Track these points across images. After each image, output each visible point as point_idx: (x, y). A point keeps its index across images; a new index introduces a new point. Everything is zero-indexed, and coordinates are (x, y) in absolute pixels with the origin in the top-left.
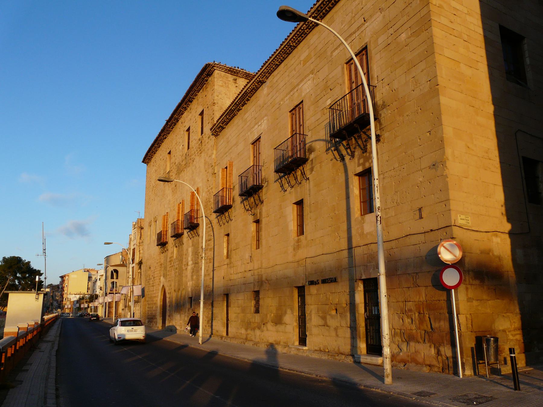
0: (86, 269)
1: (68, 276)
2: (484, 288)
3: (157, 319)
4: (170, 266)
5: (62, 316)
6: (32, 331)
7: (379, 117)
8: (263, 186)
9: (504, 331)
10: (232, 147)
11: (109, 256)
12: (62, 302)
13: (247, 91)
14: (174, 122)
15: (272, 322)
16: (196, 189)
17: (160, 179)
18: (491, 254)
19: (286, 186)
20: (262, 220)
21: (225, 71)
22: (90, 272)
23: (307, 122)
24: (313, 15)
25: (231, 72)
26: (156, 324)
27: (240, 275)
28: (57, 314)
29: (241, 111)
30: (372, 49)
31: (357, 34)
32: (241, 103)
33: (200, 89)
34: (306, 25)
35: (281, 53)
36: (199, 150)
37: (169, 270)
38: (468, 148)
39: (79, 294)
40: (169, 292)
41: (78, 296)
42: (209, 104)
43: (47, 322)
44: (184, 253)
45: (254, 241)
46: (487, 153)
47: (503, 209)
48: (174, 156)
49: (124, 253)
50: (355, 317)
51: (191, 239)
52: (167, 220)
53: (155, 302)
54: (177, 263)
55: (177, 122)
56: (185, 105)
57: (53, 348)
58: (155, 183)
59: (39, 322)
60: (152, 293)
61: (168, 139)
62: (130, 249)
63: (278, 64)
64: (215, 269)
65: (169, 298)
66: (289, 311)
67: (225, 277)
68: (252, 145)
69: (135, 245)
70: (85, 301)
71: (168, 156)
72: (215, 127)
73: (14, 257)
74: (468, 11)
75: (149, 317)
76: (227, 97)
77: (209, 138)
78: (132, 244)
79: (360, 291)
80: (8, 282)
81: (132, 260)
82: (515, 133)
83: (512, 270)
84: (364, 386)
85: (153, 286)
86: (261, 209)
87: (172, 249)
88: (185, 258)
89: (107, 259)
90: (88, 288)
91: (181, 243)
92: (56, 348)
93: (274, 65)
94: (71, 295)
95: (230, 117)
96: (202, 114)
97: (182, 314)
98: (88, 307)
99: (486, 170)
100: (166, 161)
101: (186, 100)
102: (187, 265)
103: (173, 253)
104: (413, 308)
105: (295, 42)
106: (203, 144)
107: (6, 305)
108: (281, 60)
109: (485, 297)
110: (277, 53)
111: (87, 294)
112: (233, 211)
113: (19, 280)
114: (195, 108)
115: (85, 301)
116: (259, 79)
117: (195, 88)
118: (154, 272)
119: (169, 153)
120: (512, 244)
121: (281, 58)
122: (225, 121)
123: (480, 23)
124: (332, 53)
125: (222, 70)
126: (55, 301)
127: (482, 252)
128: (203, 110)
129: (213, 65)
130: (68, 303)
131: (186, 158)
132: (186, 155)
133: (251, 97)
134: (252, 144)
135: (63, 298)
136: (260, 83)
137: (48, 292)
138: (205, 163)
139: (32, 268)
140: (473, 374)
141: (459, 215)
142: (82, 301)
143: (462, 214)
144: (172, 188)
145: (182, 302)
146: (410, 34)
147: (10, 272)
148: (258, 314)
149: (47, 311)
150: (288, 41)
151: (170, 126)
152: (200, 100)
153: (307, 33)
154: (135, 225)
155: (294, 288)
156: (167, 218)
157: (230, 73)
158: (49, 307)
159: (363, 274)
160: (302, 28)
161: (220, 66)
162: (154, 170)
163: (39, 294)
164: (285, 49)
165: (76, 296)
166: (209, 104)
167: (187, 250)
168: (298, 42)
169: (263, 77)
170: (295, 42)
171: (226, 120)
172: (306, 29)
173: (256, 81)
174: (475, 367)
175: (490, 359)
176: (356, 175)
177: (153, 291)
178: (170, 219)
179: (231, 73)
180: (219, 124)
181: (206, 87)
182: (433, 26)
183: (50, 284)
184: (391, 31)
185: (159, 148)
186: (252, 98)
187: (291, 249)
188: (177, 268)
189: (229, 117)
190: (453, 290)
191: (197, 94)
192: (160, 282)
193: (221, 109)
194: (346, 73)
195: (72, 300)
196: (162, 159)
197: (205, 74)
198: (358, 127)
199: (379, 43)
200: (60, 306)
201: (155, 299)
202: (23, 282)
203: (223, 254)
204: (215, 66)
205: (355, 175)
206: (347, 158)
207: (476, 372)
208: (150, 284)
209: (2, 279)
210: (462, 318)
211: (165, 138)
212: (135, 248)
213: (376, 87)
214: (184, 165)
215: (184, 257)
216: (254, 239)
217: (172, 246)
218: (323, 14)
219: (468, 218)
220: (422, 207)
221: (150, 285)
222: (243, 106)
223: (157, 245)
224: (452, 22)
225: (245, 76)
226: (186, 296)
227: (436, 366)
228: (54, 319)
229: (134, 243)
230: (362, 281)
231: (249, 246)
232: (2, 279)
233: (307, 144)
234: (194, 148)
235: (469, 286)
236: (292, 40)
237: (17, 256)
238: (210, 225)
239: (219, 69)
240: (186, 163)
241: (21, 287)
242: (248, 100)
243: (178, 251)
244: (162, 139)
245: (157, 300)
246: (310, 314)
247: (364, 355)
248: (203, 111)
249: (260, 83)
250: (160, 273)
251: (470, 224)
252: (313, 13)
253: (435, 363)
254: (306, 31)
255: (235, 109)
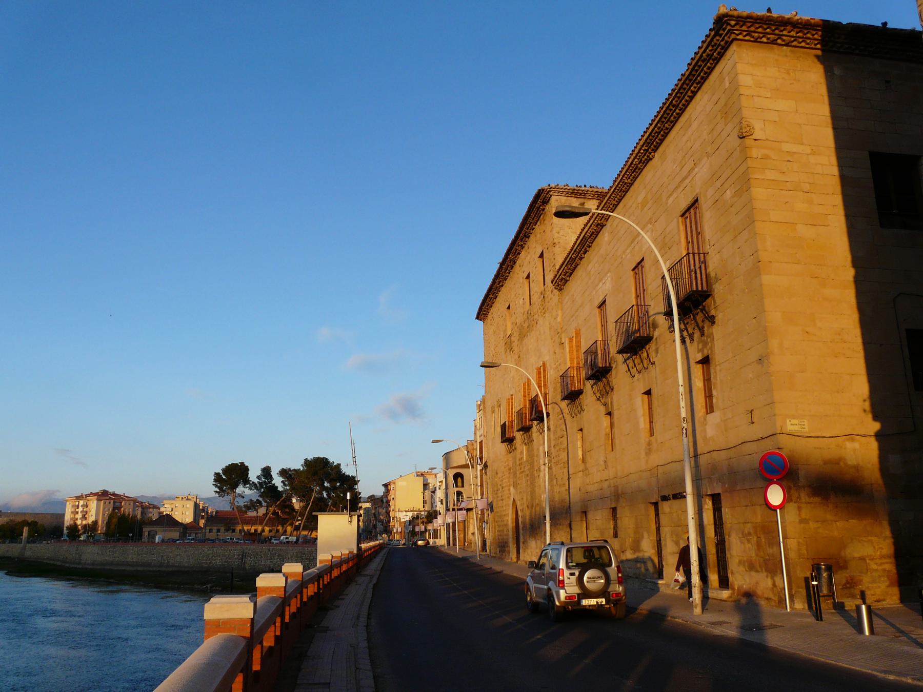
0: (419, 472)
1: (394, 483)
2: (828, 507)
3: (509, 547)
4: (520, 471)
5: (389, 545)
6: (347, 561)
7: (712, 293)
8: (612, 367)
9: (862, 559)
10: (578, 309)
11: (449, 452)
12: (389, 523)
13: (586, 236)
14: (509, 264)
15: (630, 548)
16: (542, 364)
17: (482, 365)
18: (842, 464)
19: (634, 371)
20: (613, 413)
21: (567, 195)
22: (425, 476)
23: (650, 287)
24: (643, 149)
25: (575, 195)
26: (509, 555)
27: (596, 487)
28: (381, 541)
29: (583, 260)
30: (703, 204)
31: (687, 181)
32: (581, 250)
33: (537, 221)
34: (638, 159)
35: (616, 191)
36: (542, 308)
37: (519, 478)
38: (806, 334)
39: (411, 511)
40: (521, 508)
41: (410, 514)
42: (549, 243)
43: (366, 552)
44: (536, 454)
45: (609, 440)
46: (839, 334)
47: (867, 405)
48: (514, 313)
49: (469, 448)
50: (704, 540)
51: (541, 434)
52: (512, 405)
53: (505, 523)
54: (528, 467)
55: (514, 264)
56: (521, 241)
57: (371, 581)
58: (495, 350)
59: (355, 552)
60: (501, 509)
61: (506, 287)
62: (476, 442)
63: (616, 203)
64: (570, 476)
65: (522, 517)
66: (646, 535)
67: (581, 488)
68: (599, 309)
69: (481, 435)
70: (420, 521)
71: (506, 312)
72: (556, 279)
73: (318, 458)
74: (812, 150)
75: (500, 545)
76: (572, 232)
77: (552, 292)
78: (478, 434)
79: (708, 509)
80: (314, 494)
81: (480, 459)
82: (901, 293)
83: (880, 481)
84: (671, 617)
85: (502, 500)
86: (612, 398)
87: (521, 448)
88: (536, 461)
89: (445, 457)
90: (424, 501)
91: (531, 440)
92: (374, 581)
93: (611, 204)
94: (400, 513)
95: (572, 267)
96: (541, 256)
97: (538, 539)
98: (426, 530)
99: (836, 357)
100: (505, 320)
101: (521, 235)
102: (540, 471)
103: (522, 453)
104: (751, 531)
105: (629, 178)
106: (546, 301)
107: (316, 529)
108: (618, 199)
109: (829, 517)
110: (612, 190)
111: (423, 511)
112: (585, 398)
113: (328, 492)
114: (533, 247)
115: (420, 521)
116: (597, 221)
117: (530, 220)
118: (502, 480)
119: (509, 308)
120: (881, 449)
121: (618, 196)
122: (567, 272)
123: (834, 160)
124: (667, 200)
125: (562, 195)
126: (379, 522)
127: (826, 462)
128: (543, 252)
129: (548, 190)
130: (397, 525)
131: (528, 318)
132: (528, 313)
133: (592, 243)
134: (599, 307)
135: (390, 517)
136: (599, 226)
137: (368, 507)
138: (550, 328)
139: (344, 474)
140: (807, 608)
141: (788, 421)
142: (417, 521)
143: (794, 419)
144: (515, 360)
145: (536, 523)
146: (733, 192)
147: (315, 480)
148: (617, 539)
149: (367, 537)
150: (621, 177)
151: (506, 270)
152: (538, 236)
153: (634, 179)
154: (480, 406)
155: (649, 504)
156: (512, 402)
157: (574, 196)
158: (372, 532)
159: (708, 487)
160: (634, 163)
161: (558, 190)
162: (492, 330)
163: (352, 515)
164: (619, 186)
165: (408, 513)
166: (549, 243)
167: (538, 449)
168: (633, 178)
169: (601, 219)
170: (629, 178)
171: (568, 271)
172: (639, 163)
173: (594, 224)
174: (811, 601)
175: (821, 590)
176: (698, 362)
177: (503, 507)
178: (515, 404)
179: (576, 196)
180: (560, 275)
181: (543, 217)
182: (753, 187)
183: (371, 495)
184: (718, 184)
185: (495, 299)
186: (594, 243)
187: (643, 455)
188: (528, 474)
189: (571, 266)
190: (778, 510)
191: (534, 227)
192: (510, 494)
193: (564, 251)
194: (682, 228)
195: (402, 520)
196: (500, 317)
197: (540, 202)
198: (690, 305)
199: (709, 197)
200: (387, 530)
201: (505, 518)
202: (334, 495)
203: (578, 456)
204: (551, 191)
205: (696, 363)
206: (688, 340)
207: (812, 607)
208: (498, 497)
209: (306, 490)
210: (792, 543)
211: (502, 286)
212: (482, 441)
213: (708, 253)
214: (526, 327)
215: (536, 458)
216: (608, 438)
217: (520, 443)
218: (655, 146)
219: (804, 422)
220: (752, 410)
221: (499, 499)
222: (585, 253)
223: (502, 442)
224: (784, 173)
225: (596, 196)
226: (541, 515)
227: (773, 600)
228: (377, 548)
229: (480, 434)
230: (710, 497)
231: (603, 447)
232: (306, 490)
233: (650, 316)
234: (537, 304)
235: (803, 505)
236: (626, 176)
237: (322, 457)
238: (562, 416)
239: (557, 194)
240: (529, 325)
241: (331, 501)
242: (589, 247)
243: (528, 450)
244: (497, 287)
245: (508, 521)
246: (665, 540)
247: (716, 589)
248: (542, 253)
249: (599, 226)
250: (509, 481)
251: (807, 429)
252: (643, 146)
253: (771, 596)
254: (639, 166)
255: (576, 258)
